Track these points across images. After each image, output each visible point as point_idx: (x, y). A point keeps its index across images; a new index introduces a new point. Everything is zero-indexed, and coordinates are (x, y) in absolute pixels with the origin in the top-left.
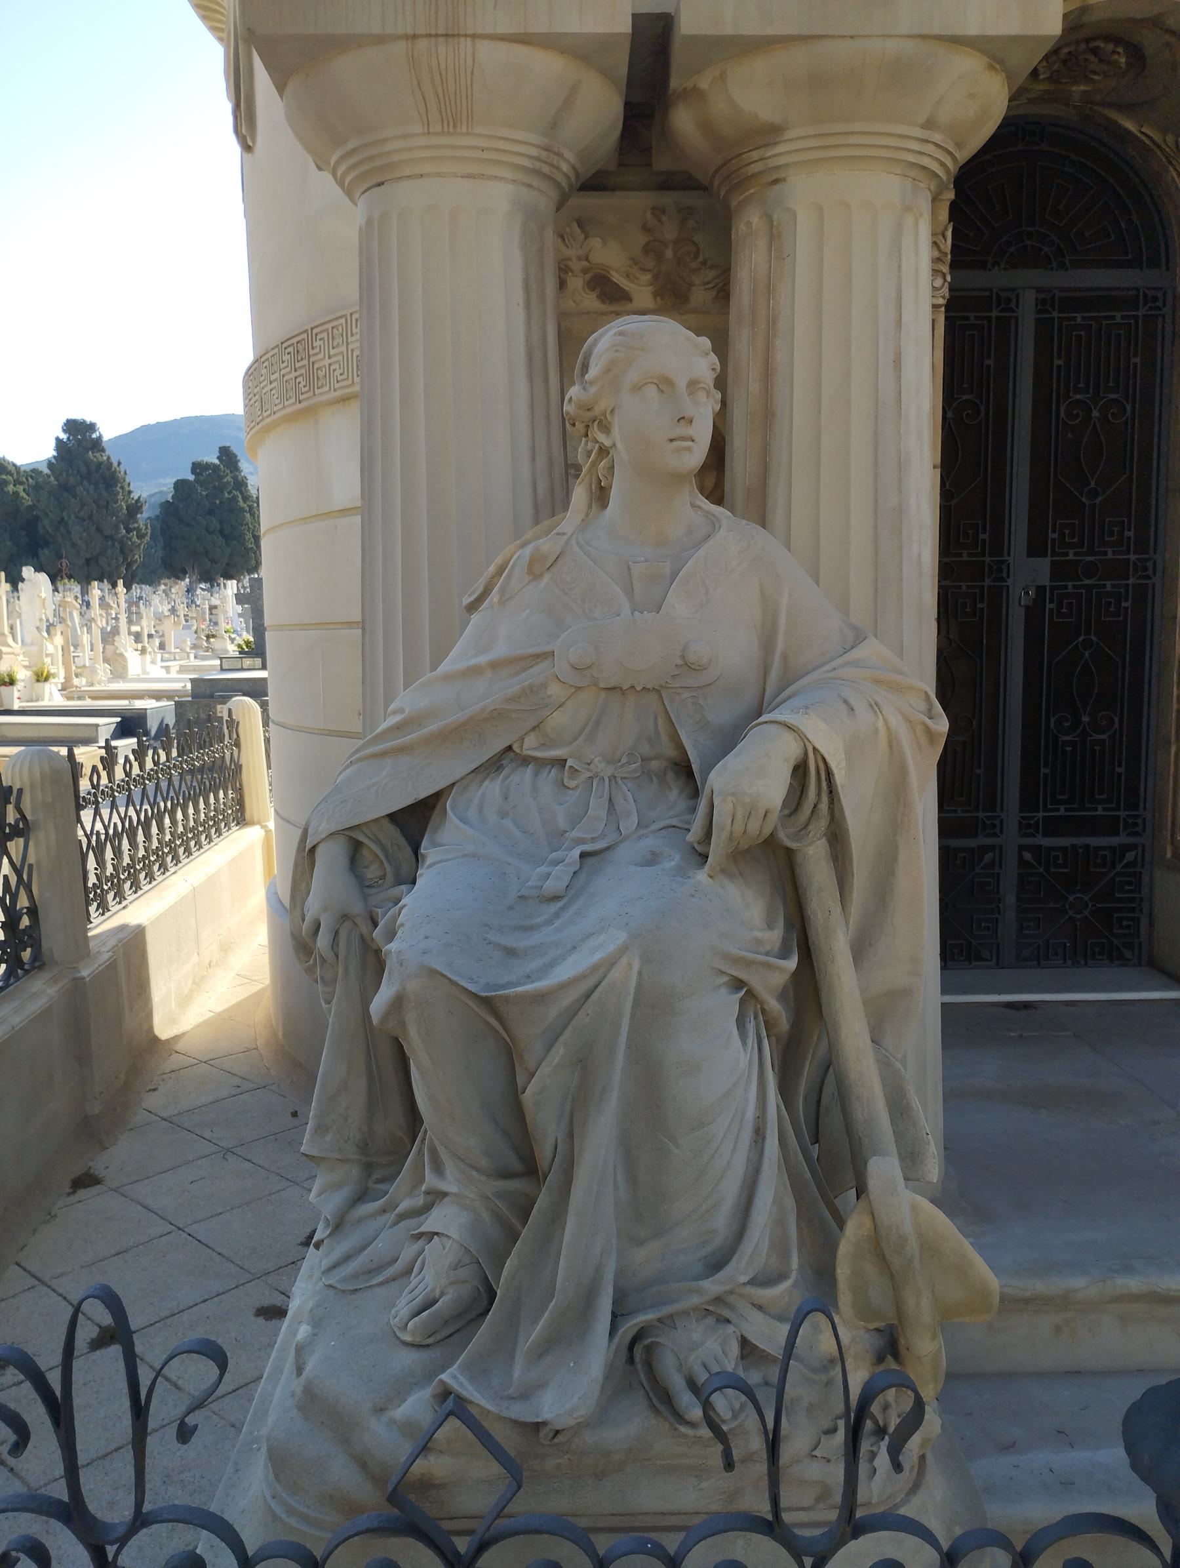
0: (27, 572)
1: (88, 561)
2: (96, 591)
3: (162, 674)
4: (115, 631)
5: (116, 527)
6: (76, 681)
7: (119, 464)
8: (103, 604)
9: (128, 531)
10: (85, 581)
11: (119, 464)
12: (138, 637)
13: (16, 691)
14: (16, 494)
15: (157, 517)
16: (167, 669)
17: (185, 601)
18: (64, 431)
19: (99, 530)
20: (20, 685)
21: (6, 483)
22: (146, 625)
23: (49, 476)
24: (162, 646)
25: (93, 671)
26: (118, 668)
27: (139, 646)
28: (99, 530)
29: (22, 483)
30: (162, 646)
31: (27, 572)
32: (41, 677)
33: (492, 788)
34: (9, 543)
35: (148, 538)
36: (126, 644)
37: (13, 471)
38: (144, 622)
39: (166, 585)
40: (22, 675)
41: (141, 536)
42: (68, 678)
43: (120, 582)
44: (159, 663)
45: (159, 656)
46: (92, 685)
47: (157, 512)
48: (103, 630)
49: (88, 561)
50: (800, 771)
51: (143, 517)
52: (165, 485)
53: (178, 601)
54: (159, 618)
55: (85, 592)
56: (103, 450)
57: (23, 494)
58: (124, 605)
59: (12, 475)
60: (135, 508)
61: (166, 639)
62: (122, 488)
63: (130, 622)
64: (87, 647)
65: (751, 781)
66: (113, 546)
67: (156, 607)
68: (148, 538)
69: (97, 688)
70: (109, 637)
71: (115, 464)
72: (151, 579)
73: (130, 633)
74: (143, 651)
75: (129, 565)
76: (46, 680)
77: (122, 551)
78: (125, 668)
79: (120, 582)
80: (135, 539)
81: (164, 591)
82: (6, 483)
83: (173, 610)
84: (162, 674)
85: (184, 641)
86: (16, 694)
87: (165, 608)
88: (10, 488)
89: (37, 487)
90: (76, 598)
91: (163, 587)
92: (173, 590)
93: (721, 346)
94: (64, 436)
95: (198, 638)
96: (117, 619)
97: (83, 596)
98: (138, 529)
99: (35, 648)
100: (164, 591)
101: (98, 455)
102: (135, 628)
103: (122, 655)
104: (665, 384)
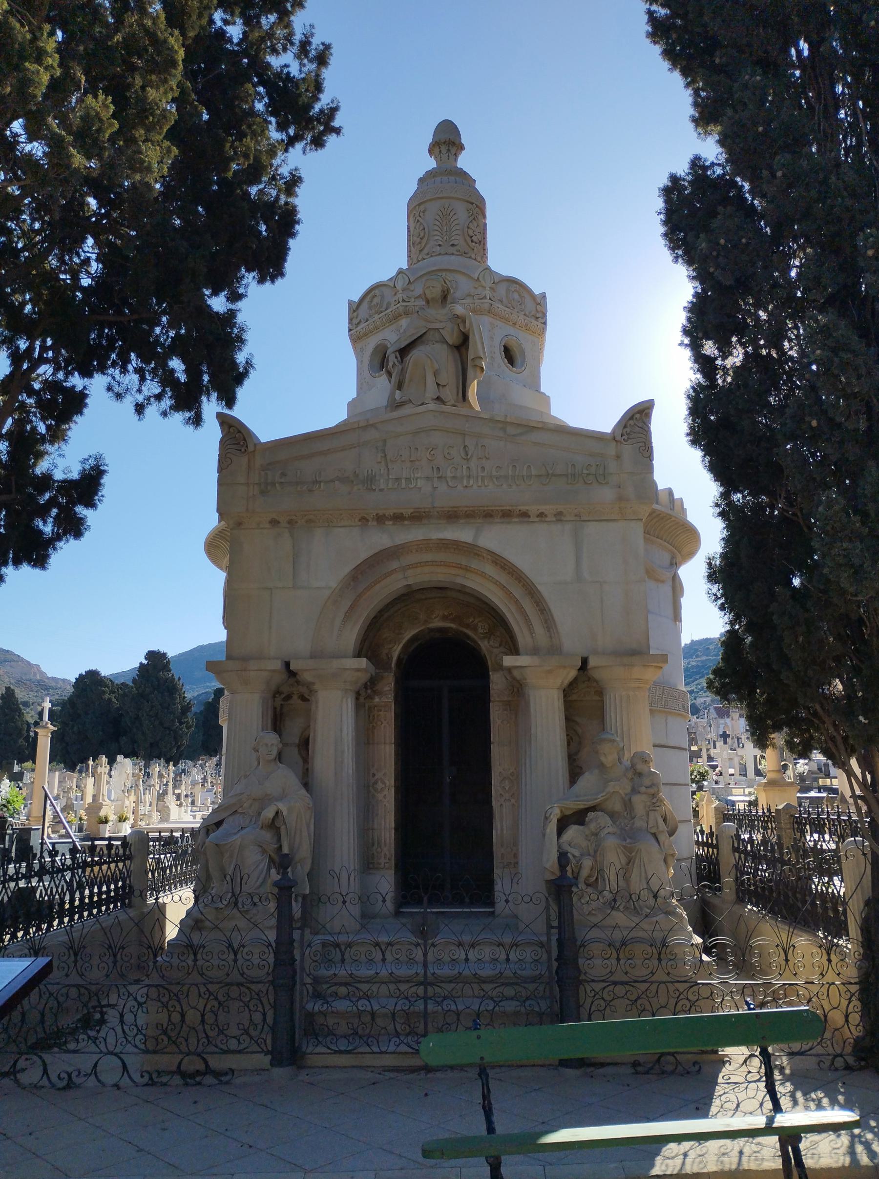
0: (120, 758)
1: (151, 744)
2: (156, 768)
3: (191, 819)
4: (165, 793)
5: (173, 721)
6: (140, 823)
7: (179, 679)
8: (160, 776)
9: (181, 723)
10: (149, 758)
11: (179, 679)
12: (178, 797)
13: (108, 827)
14: (110, 700)
15: (201, 712)
16: (194, 817)
17: (214, 772)
18: (146, 658)
19: (161, 724)
20: (110, 824)
21: (104, 692)
22: (183, 790)
23: (132, 687)
24: (193, 803)
25: (150, 816)
26: (165, 818)
27: (179, 803)
28: (161, 724)
29: (114, 693)
30: (193, 803)
31: (120, 758)
32: (122, 819)
33: (231, 818)
34: (101, 733)
35: (193, 728)
36: (170, 800)
37: (108, 682)
38: (183, 787)
39: (203, 760)
40: (112, 817)
41: (188, 728)
42: (135, 820)
43: (171, 763)
44: (189, 813)
45: (190, 808)
46: (149, 825)
47: (202, 708)
48: (158, 792)
49: (151, 744)
50: (277, 813)
51: (190, 718)
52: (210, 687)
53: (209, 772)
54: (194, 783)
55: (147, 766)
56: (170, 671)
57: (114, 700)
58: (172, 775)
59: (108, 687)
60: (186, 709)
61: (196, 798)
62: (180, 695)
63: (175, 787)
64: (148, 804)
65: (269, 813)
66: (169, 734)
67: (194, 776)
68: (193, 728)
69: (151, 826)
70: (161, 796)
71: (177, 679)
72: (193, 756)
73: (174, 794)
74: (180, 805)
75: (179, 747)
76: (124, 821)
77: (175, 738)
78: (168, 815)
79: (171, 763)
80: (185, 730)
81: (201, 765)
82: (104, 692)
83: (205, 780)
84: (191, 819)
85: (207, 799)
86: (108, 829)
87: (199, 778)
88: (107, 696)
89: (125, 695)
90: (141, 770)
91: (200, 762)
92: (207, 764)
93: (280, 736)
94: (145, 662)
95: (216, 797)
96: (166, 785)
97: (145, 769)
98: (187, 722)
99: (120, 803)
100: (201, 765)
101: (166, 673)
102: (177, 791)
103: (168, 807)
104: (267, 745)
